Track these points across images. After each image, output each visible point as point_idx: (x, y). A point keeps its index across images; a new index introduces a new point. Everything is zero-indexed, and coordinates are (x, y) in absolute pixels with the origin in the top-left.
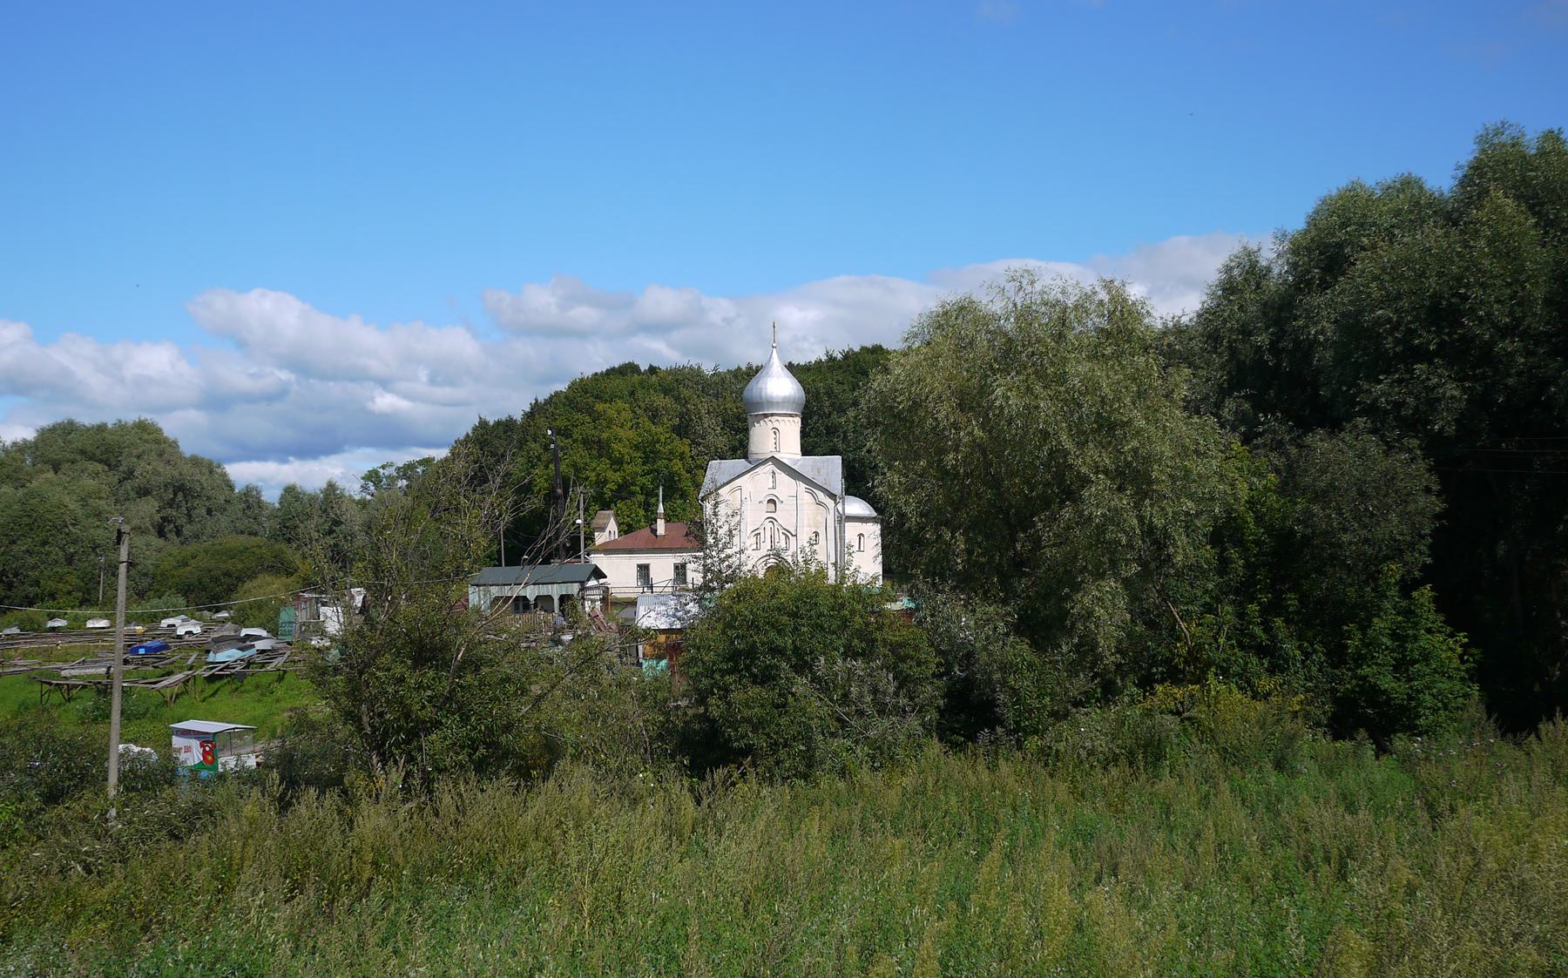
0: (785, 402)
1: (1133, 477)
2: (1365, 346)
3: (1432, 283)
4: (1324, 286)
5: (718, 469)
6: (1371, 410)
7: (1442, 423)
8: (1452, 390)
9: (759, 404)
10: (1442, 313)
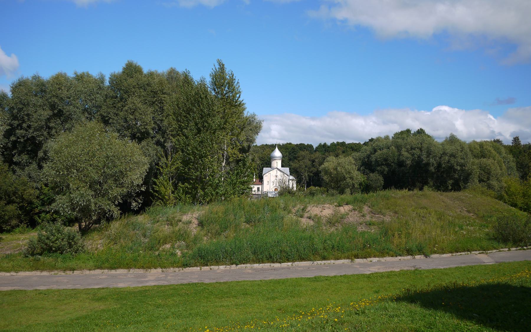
0: (279, 157)
1: (352, 178)
2: (378, 163)
3: (385, 156)
4: (374, 154)
5: (265, 170)
6: (378, 171)
7: (385, 173)
8: (386, 169)
9: (274, 157)
10: (386, 160)
